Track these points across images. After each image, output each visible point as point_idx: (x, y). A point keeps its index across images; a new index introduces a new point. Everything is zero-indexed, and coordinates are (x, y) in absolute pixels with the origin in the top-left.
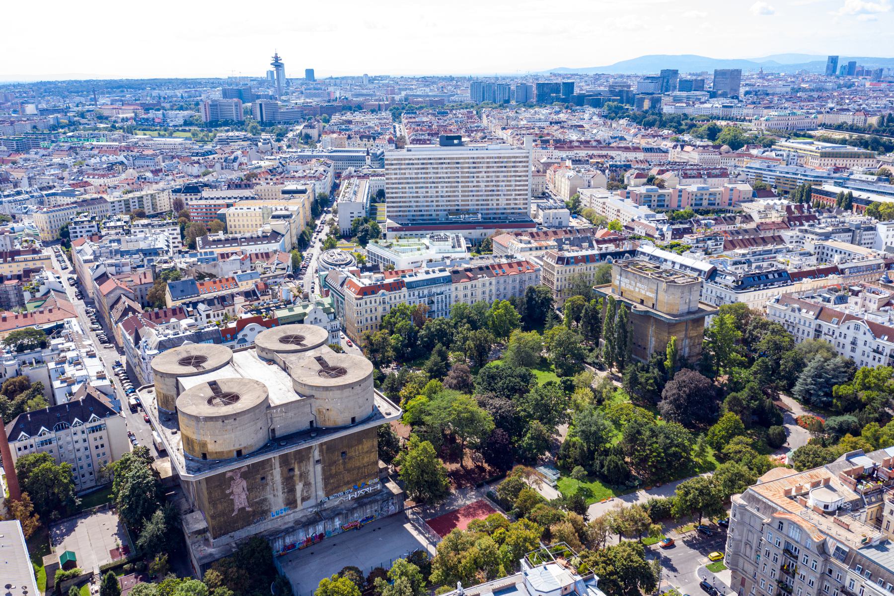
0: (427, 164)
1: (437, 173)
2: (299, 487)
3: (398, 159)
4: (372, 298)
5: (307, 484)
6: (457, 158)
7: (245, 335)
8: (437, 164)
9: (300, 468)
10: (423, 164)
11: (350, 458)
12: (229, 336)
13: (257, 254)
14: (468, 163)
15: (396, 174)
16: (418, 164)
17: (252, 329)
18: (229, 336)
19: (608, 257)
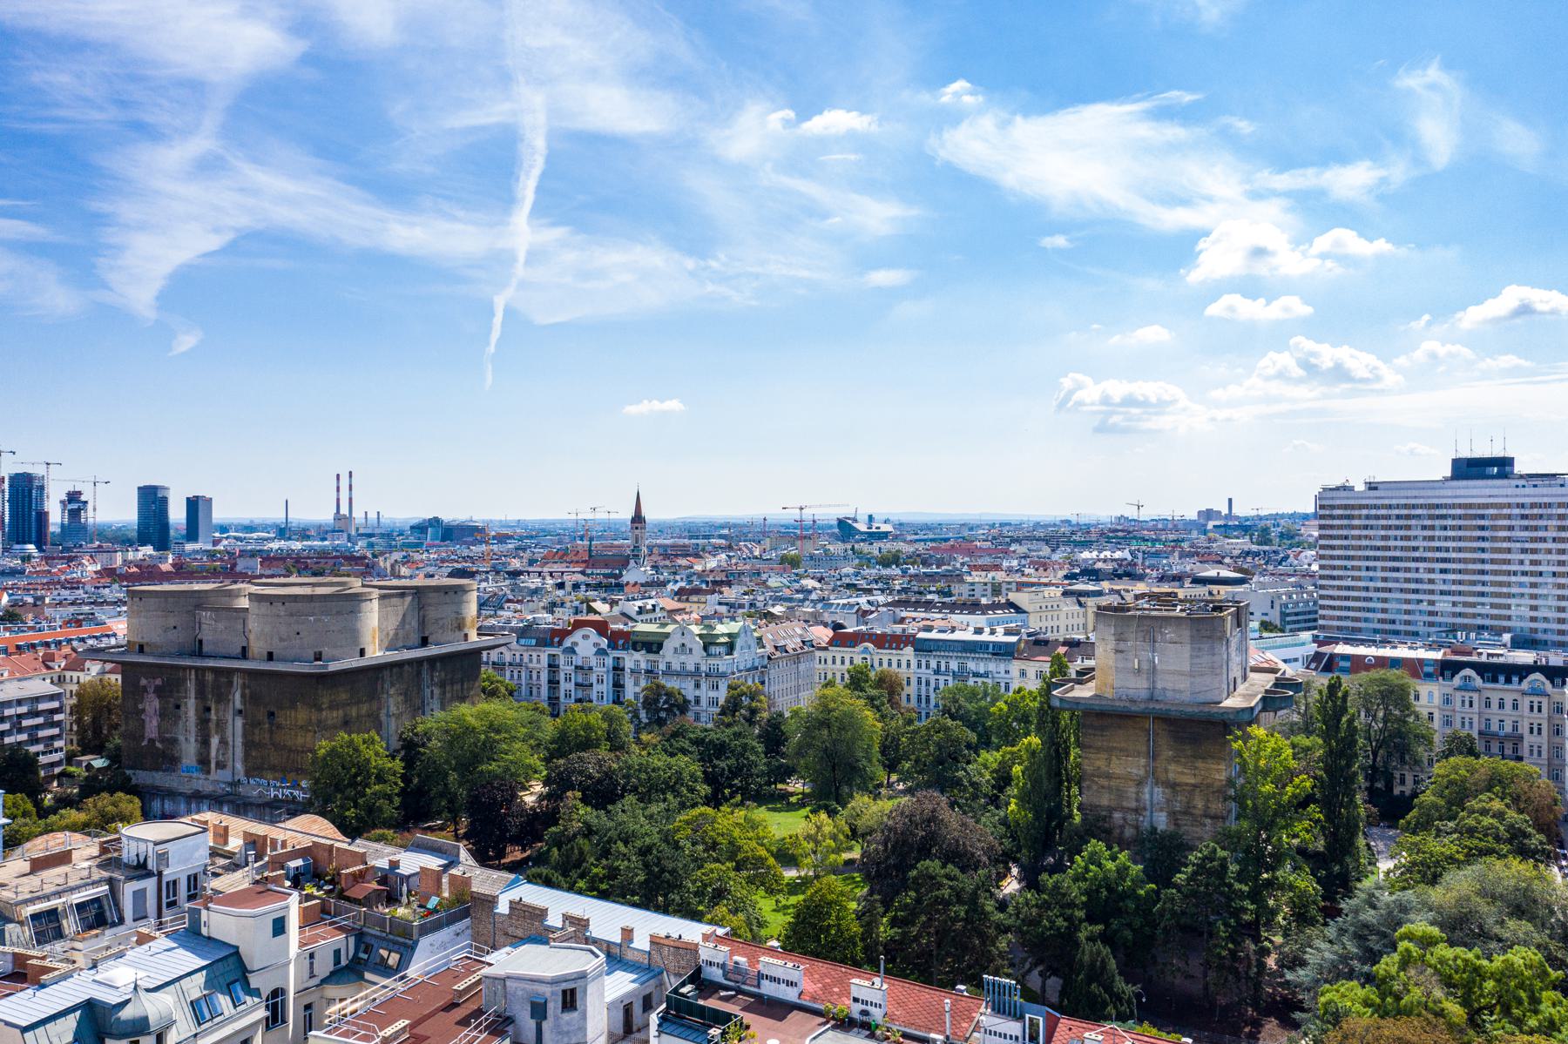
0: (1408, 517)
1: (1432, 538)
2: (215, 741)
3: (1346, 507)
5: (223, 742)
6: (1480, 506)
7: (576, 644)
8: (1431, 517)
9: (217, 711)
10: (1398, 517)
11: (279, 727)
14: (1509, 517)
15: (1511, 528)
16: (1388, 517)
17: (585, 637)
19: (1468, 672)
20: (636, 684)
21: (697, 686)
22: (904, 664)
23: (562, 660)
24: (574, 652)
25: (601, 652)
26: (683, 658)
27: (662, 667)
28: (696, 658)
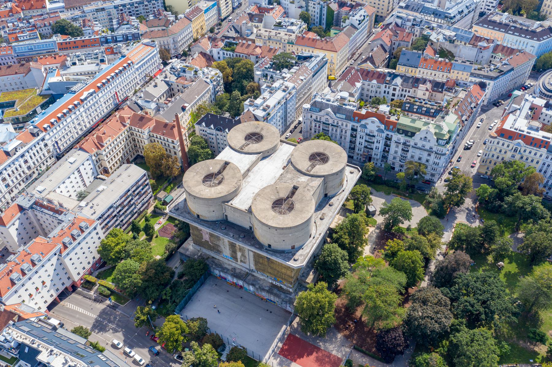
4: (507, 142)
5: (243, 255)
7: (368, 124)
12: (357, 118)
13: (504, 47)
18: (357, 118)
20: (397, 147)
21: (429, 155)
22: (538, 155)
23: (359, 129)
24: (366, 128)
25: (380, 131)
26: (424, 143)
27: (412, 143)
28: (432, 143)
